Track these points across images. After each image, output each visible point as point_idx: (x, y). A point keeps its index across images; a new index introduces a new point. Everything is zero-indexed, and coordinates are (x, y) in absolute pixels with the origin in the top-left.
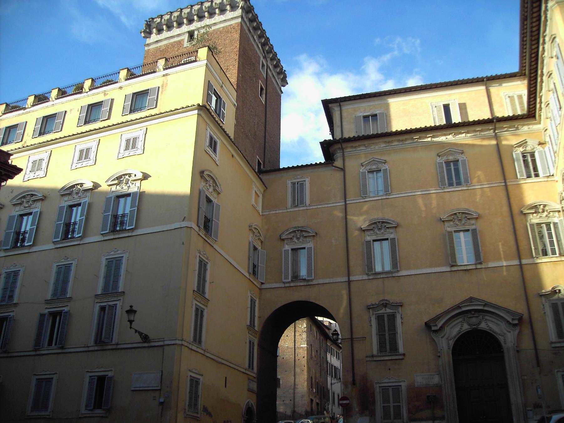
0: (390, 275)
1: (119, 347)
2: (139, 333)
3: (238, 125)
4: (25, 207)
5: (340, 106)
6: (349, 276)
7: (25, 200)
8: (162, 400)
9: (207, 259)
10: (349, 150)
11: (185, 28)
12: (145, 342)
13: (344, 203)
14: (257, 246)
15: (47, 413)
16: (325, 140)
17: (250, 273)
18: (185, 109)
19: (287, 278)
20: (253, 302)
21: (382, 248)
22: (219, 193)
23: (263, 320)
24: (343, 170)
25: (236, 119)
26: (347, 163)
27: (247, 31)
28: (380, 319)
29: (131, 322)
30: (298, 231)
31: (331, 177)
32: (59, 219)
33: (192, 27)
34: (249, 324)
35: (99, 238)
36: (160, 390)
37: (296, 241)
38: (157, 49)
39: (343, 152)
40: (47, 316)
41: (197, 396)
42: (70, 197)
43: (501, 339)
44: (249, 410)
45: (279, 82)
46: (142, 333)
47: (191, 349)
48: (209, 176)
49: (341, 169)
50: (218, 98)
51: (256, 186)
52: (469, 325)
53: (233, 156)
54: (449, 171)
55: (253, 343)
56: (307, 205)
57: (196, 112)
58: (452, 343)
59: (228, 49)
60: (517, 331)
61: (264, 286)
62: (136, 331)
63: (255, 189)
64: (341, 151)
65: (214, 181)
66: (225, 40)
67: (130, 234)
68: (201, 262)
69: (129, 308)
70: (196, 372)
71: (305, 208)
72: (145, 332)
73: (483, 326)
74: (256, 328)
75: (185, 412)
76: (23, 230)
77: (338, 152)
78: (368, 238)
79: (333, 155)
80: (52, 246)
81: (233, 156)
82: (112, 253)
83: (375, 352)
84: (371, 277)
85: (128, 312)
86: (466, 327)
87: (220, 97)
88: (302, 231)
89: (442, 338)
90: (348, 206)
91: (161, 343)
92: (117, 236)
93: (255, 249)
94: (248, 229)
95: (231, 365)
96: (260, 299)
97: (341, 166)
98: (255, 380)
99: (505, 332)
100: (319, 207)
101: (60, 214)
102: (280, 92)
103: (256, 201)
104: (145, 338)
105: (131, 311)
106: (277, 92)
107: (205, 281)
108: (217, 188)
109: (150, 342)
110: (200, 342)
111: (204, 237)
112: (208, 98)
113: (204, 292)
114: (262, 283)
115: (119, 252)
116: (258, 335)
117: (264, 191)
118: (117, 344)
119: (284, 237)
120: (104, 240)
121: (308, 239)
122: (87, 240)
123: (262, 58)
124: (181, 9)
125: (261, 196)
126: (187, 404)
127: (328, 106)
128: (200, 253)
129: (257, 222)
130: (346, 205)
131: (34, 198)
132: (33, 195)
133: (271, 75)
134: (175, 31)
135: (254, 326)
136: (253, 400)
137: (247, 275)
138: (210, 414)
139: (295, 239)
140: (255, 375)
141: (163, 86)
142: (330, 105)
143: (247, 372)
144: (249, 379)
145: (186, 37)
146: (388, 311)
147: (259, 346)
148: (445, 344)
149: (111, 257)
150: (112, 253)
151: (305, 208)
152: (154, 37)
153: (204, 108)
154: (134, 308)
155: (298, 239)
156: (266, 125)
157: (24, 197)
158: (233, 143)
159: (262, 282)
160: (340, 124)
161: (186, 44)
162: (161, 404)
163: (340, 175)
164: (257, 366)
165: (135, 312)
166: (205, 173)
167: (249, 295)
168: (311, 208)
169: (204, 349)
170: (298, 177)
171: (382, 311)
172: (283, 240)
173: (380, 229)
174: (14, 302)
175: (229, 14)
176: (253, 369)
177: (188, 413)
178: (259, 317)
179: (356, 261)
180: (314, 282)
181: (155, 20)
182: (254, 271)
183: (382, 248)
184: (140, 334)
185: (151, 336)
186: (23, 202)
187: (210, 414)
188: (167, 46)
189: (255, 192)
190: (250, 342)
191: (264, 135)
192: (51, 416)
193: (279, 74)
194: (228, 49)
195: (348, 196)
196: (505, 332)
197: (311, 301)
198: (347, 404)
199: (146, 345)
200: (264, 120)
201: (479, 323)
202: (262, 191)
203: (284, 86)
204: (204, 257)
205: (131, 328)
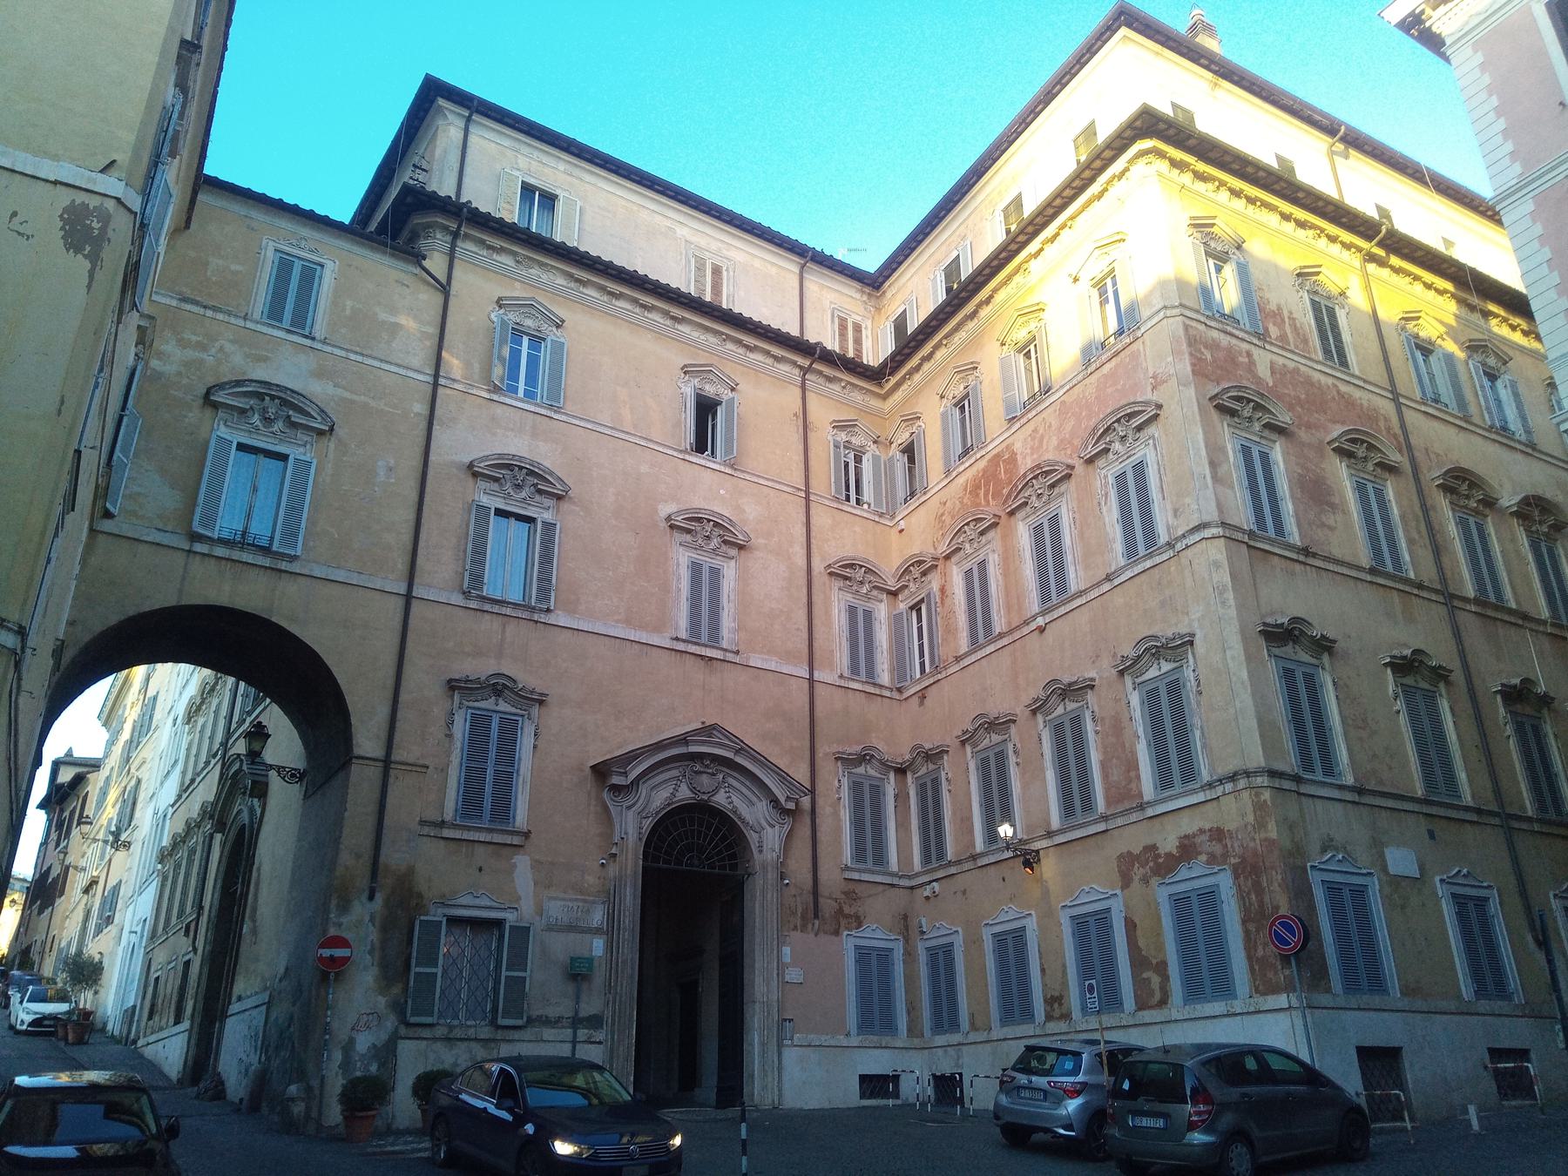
43: (753, 838)
52: (693, 789)
58: (647, 824)
60: (787, 828)
73: (720, 799)
86: (684, 793)
89: (629, 808)
99: (764, 824)
148: (632, 826)
196: (764, 824)
201: (716, 791)
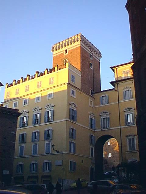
0: (132, 126)
5: (35, 152)
6: (120, 126)
8: (63, 168)
10: (120, 84)
11: (64, 49)
17: (90, 128)
18: (63, 84)
19: (102, 127)
21: (130, 116)
28: (130, 139)
29: (53, 148)
31: (114, 93)
33: (67, 48)
38: (57, 56)
42: (36, 112)
44: (92, 169)
49: (117, 91)
54: (104, 121)
59: (77, 56)
61: (95, 131)
62: (55, 150)
63: (90, 100)
69: (52, 145)
72: (57, 150)
75: (38, 180)
76: (24, 121)
78: (126, 114)
81: (81, 93)
83: (128, 150)
84: (127, 127)
85: (52, 146)
92: (49, 123)
97: (117, 90)
101: (33, 117)
103: (91, 104)
104: (58, 152)
105: (53, 145)
119: (100, 115)
124: (62, 41)
130: (119, 103)
131: (26, 112)
132: (25, 111)
133: (95, 57)
134: (61, 50)
136: (93, 166)
139: (104, 115)
145: (65, 52)
146: (132, 137)
147: (95, 149)
152: (55, 52)
154: (54, 144)
155: (105, 115)
158: (81, 90)
161: (65, 54)
162: (63, 169)
165: (54, 145)
171: (130, 137)
172: (100, 115)
173: (129, 111)
175: (77, 43)
176: (93, 156)
179: (123, 120)
180: (110, 129)
181: (55, 45)
183: (130, 116)
188: (59, 55)
194: (77, 56)
197: (109, 134)
199: (58, 153)
205: (53, 150)
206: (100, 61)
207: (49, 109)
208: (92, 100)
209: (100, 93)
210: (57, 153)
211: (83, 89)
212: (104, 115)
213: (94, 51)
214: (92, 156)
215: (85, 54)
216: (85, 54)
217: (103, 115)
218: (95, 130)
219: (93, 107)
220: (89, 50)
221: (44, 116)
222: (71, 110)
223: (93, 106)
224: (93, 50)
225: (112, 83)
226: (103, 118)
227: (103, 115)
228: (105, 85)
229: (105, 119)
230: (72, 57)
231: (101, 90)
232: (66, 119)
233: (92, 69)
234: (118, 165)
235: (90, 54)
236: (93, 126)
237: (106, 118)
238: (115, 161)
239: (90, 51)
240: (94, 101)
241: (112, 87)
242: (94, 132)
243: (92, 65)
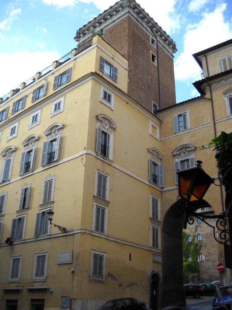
1: (52, 236)
2: (58, 226)
3: (130, 83)
4: (8, 157)
7: (7, 153)
8: (72, 270)
9: (107, 174)
10: (214, 85)
12: (64, 232)
13: (213, 123)
14: (157, 163)
15: (18, 280)
16: (196, 81)
17: (150, 182)
20: (155, 202)
22: (114, 129)
23: (165, 213)
24: (211, 100)
25: (129, 78)
26: (213, 94)
27: (135, 21)
30: (184, 148)
32: (22, 161)
34: (151, 216)
35: (42, 169)
36: (72, 263)
37: (183, 155)
39: (210, 88)
40: (17, 221)
41: (101, 268)
44: (155, 276)
45: (171, 51)
46: (61, 227)
47: (94, 236)
48: (104, 118)
50: (111, 65)
51: (152, 122)
53: (127, 103)
55: (157, 230)
56: (189, 129)
57: (91, 78)
61: (164, 190)
62: (55, 226)
63: (151, 123)
64: (209, 87)
65: (109, 121)
66: (120, 29)
67: (56, 164)
68: (100, 176)
70: (100, 251)
71: (187, 131)
72: (63, 225)
74: (159, 219)
77: (207, 88)
79: (204, 90)
80: (19, 178)
81: (127, 103)
82: (48, 177)
87: (112, 66)
88: (186, 148)
90: (216, 125)
91: (72, 233)
93: (155, 165)
94: (146, 151)
95: (135, 245)
96: (161, 199)
97: (210, 97)
98: (161, 255)
100: (197, 129)
102: (171, 57)
103: (154, 132)
104: (64, 230)
106: (169, 57)
107: (104, 188)
108: (112, 125)
109: (66, 233)
110: (102, 230)
111: (102, 159)
112: (101, 68)
113: (104, 196)
114: (163, 188)
115: (51, 176)
116: (161, 225)
117: (161, 124)
118: (50, 235)
119: (175, 153)
120: (44, 170)
121: (190, 153)
122: (35, 172)
123: (151, 36)
125: (158, 128)
126: (92, 272)
127: (198, 58)
128: (99, 170)
129: (153, 144)
130: (215, 124)
135: (157, 217)
136: (159, 269)
137: (148, 183)
138: (115, 279)
139: (182, 154)
140: (160, 252)
141: (74, 66)
142: (199, 57)
143: (151, 250)
144: (153, 254)
147: (162, 231)
149: (47, 180)
150: (48, 177)
151: (187, 131)
153: (95, 74)
155: (184, 153)
156: (159, 80)
157: (7, 151)
158: (128, 96)
159: (162, 186)
160: (206, 69)
162: (73, 272)
163: (209, 104)
164: (162, 245)
166: (99, 117)
167: (151, 196)
168: (192, 130)
169: (107, 235)
170: (182, 110)
174: (3, 214)
176: (157, 247)
177: (92, 278)
178: (162, 211)
182: (155, 179)
184: (59, 227)
185: (68, 228)
186: (7, 154)
187: (115, 279)
189: (152, 125)
190: (154, 229)
191: (158, 86)
192: (19, 282)
193: (169, 45)
195: (216, 118)
198: (222, 269)
200: (157, 76)
202: (159, 124)
203: (174, 52)
204: (103, 173)
206: (174, 57)
207: (54, 135)
208: (158, 125)
209: (172, 110)
210: (61, 235)
211: (131, 96)
212: (182, 154)
213: (159, 33)
214: (155, 244)
215: (140, 34)
216: (140, 34)
217: (180, 154)
218: (163, 188)
219: (159, 140)
220: (149, 29)
221: (42, 152)
222: (99, 134)
223: (158, 136)
224: (157, 32)
225: (198, 85)
226: (181, 162)
227: (180, 154)
228: (185, 91)
229: (186, 162)
230: (111, 39)
231: (178, 102)
232: (85, 152)
233: (156, 65)
234: (217, 157)
235: (151, 36)
236: (159, 179)
237: (188, 160)
238: (211, 267)
239: (151, 32)
240: (160, 127)
241: (196, 93)
242: (162, 192)
243: (156, 58)
